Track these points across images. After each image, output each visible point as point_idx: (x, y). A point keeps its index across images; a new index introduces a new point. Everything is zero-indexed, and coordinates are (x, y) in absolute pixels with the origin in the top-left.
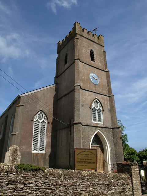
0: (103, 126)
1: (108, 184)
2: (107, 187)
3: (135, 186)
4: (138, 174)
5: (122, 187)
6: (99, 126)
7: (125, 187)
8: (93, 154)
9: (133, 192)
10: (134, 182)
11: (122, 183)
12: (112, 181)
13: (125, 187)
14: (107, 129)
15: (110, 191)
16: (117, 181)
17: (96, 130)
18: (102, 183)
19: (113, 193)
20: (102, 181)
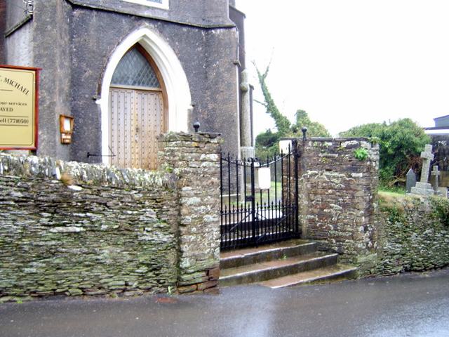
0: (165, 17)
1: (53, 202)
2: (45, 211)
3: (190, 214)
4: (213, 174)
5: (123, 214)
6: (146, 14)
7: (141, 218)
8: (18, 91)
9: (178, 234)
10: (52, 195)
11: (127, 200)
12: (73, 191)
13: (141, 218)
14: (185, 29)
15: (64, 225)
16: (104, 194)
17: (132, 29)
18: (20, 194)
19: (78, 233)
20: (20, 189)
